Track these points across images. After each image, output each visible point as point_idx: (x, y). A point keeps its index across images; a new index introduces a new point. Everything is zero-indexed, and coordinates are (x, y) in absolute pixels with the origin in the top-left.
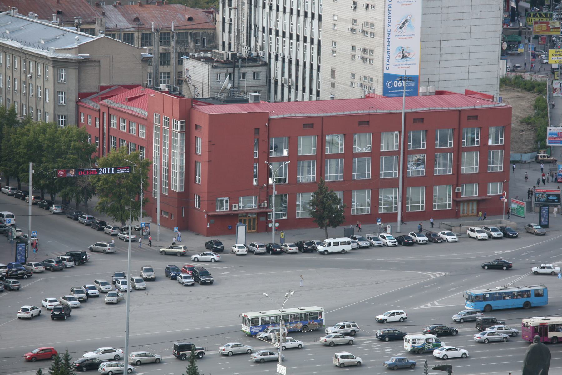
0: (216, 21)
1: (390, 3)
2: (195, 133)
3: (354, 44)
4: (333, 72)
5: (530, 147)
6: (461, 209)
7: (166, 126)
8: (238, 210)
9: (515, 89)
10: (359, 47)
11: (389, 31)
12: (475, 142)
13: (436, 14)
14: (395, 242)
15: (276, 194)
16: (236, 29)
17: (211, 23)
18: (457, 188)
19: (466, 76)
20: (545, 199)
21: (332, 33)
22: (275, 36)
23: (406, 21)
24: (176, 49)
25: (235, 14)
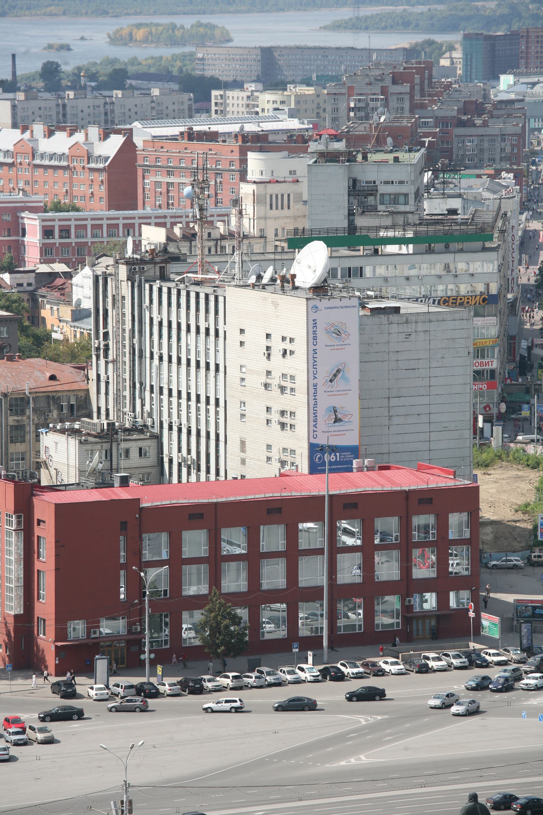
0: (88, 379)
1: (315, 347)
2: (38, 531)
3: (269, 405)
4: (243, 443)
5: (522, 545)
6: (415, 628)
7: (10, 526)
8: (100, 637)
9: (514, 466)
10: (276, 408)
11: (315, 385)
12: (431, 535)
13: (382, 361)
14: (318, 676)
15: (150, 612)
16: (115, 390)
17: (82, 383)
18: (408, 599)
19: (426, 446)
20: (529, 613)
21: (239, 391)
22: (167, 396)
23: (338, 371)
24: (33, 420)
25: (114, 368)
